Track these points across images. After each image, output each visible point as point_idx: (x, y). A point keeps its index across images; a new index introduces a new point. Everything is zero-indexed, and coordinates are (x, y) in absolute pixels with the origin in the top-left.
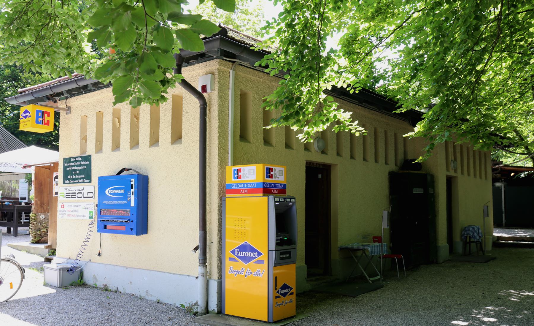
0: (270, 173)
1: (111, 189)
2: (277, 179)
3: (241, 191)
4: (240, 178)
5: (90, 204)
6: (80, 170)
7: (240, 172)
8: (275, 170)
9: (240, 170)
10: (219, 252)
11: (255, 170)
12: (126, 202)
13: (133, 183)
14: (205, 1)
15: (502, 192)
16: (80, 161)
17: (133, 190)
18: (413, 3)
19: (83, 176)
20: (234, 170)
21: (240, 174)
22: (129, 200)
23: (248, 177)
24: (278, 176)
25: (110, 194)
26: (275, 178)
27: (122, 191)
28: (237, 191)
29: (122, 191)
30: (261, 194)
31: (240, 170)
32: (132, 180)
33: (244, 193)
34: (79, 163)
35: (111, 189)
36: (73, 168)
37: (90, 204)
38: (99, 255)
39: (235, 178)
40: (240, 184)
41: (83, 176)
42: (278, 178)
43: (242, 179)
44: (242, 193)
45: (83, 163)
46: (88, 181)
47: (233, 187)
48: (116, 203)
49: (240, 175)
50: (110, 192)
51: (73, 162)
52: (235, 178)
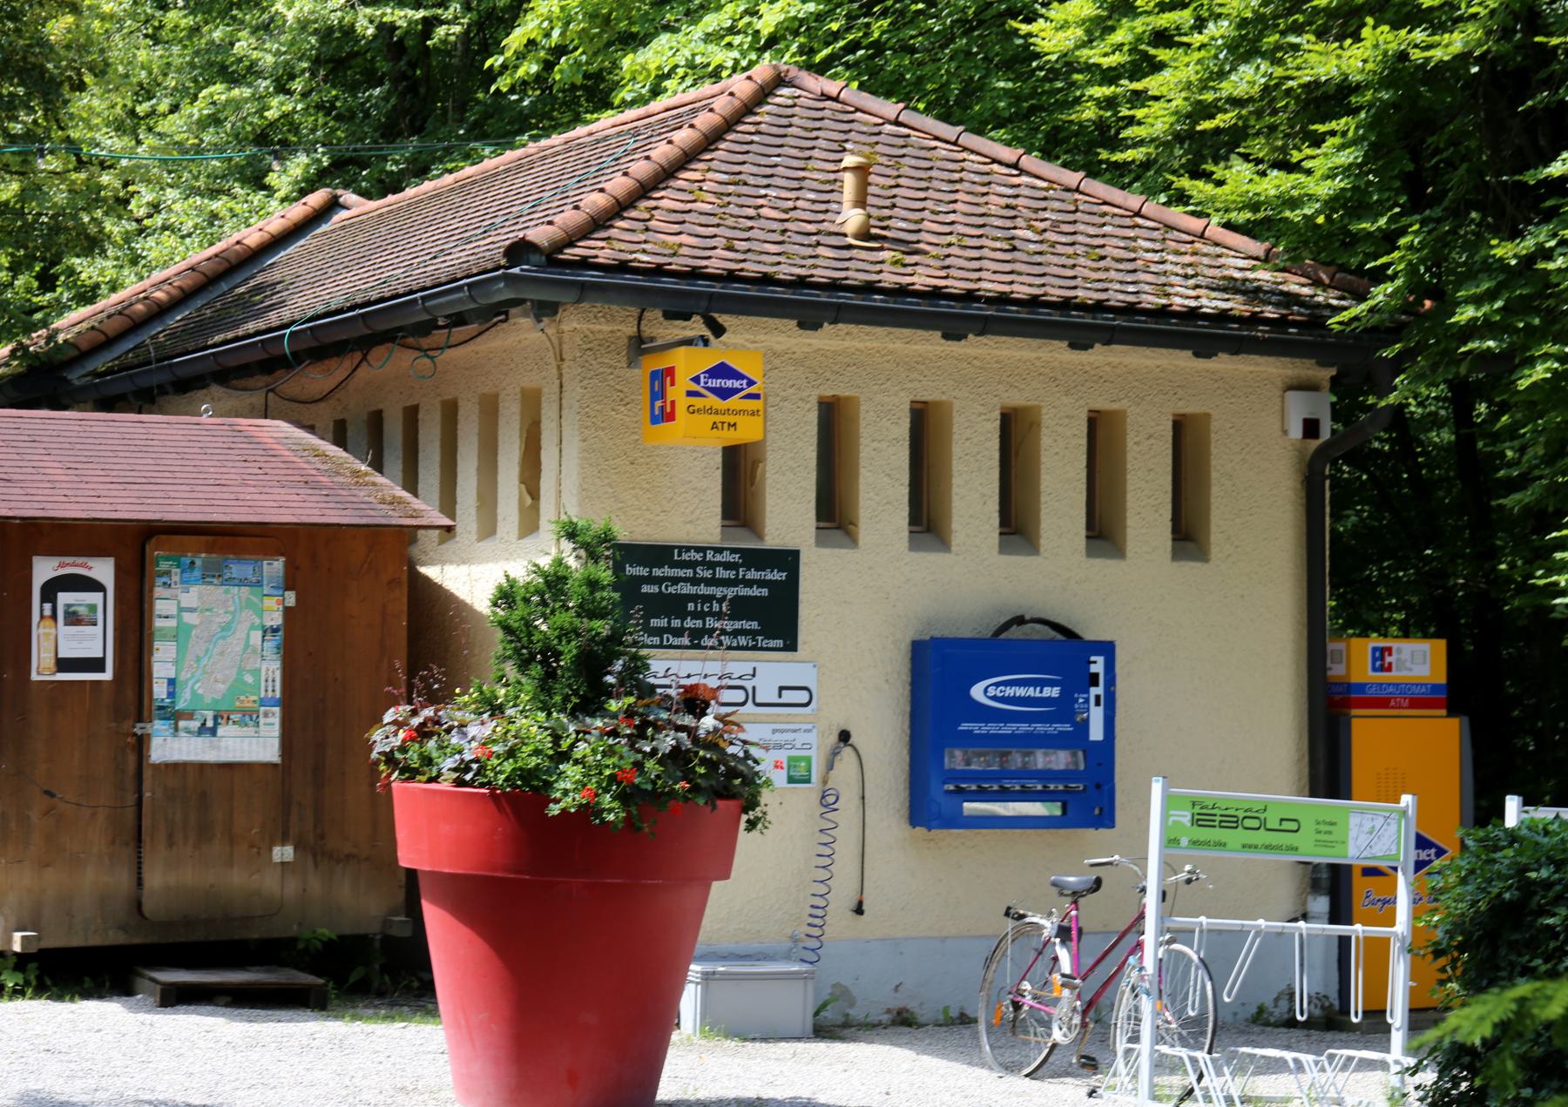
0: (1382, 659)
1: (997, 685)
2: (1404, 673)
3: (1392, 703)
4: (1389, 669)
5: (795, 731)
6: (736, 600)
7: (1390, 654)
8: (1399, 651)
9: (1389, 650)
10: (408, 988)
11: (1428, 654)
12: (1067, 728)
13: (1094, 669)
14: (1073, 4)
15: (115, 629)
16: (727, 566)
17: (1094, 691)
18: (1400, 71)
19: (754, 625)
20: (1375, 650)
21: (1388, 659)
22: (1083, 720)
23: (1410, 670)
24: (1408, 665)
25: (994, 698)
26: (1399, 669)
27: (1054, 692)
28: (1382, 703)
29: (1054, 692)
30: (1444, 712)
31: (1389, 650)
32: (1093, 658)
33: (1400, 708)
34: (722, 573)
35: (997, 685)
36: (687, 589)
37: (795, 731)
38: (859, 910)
39: (1374, 669)
40: (1389, 684)
41: (754, 625)
42: (1410, 670)
43: (1394, 673)
44: (1392, 707)
45: (752, 574)
46: (779, 643)
47: (1371, 693)
48: (1024, 727)
49: (1390, 664)
50: (992, 691)
51: (692, 565)
52: (1374, 669)
